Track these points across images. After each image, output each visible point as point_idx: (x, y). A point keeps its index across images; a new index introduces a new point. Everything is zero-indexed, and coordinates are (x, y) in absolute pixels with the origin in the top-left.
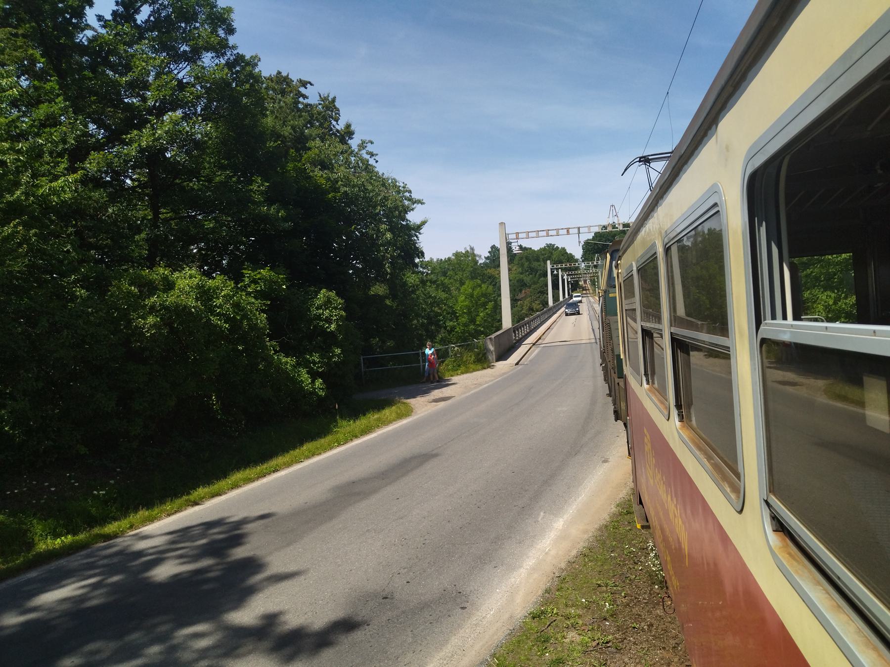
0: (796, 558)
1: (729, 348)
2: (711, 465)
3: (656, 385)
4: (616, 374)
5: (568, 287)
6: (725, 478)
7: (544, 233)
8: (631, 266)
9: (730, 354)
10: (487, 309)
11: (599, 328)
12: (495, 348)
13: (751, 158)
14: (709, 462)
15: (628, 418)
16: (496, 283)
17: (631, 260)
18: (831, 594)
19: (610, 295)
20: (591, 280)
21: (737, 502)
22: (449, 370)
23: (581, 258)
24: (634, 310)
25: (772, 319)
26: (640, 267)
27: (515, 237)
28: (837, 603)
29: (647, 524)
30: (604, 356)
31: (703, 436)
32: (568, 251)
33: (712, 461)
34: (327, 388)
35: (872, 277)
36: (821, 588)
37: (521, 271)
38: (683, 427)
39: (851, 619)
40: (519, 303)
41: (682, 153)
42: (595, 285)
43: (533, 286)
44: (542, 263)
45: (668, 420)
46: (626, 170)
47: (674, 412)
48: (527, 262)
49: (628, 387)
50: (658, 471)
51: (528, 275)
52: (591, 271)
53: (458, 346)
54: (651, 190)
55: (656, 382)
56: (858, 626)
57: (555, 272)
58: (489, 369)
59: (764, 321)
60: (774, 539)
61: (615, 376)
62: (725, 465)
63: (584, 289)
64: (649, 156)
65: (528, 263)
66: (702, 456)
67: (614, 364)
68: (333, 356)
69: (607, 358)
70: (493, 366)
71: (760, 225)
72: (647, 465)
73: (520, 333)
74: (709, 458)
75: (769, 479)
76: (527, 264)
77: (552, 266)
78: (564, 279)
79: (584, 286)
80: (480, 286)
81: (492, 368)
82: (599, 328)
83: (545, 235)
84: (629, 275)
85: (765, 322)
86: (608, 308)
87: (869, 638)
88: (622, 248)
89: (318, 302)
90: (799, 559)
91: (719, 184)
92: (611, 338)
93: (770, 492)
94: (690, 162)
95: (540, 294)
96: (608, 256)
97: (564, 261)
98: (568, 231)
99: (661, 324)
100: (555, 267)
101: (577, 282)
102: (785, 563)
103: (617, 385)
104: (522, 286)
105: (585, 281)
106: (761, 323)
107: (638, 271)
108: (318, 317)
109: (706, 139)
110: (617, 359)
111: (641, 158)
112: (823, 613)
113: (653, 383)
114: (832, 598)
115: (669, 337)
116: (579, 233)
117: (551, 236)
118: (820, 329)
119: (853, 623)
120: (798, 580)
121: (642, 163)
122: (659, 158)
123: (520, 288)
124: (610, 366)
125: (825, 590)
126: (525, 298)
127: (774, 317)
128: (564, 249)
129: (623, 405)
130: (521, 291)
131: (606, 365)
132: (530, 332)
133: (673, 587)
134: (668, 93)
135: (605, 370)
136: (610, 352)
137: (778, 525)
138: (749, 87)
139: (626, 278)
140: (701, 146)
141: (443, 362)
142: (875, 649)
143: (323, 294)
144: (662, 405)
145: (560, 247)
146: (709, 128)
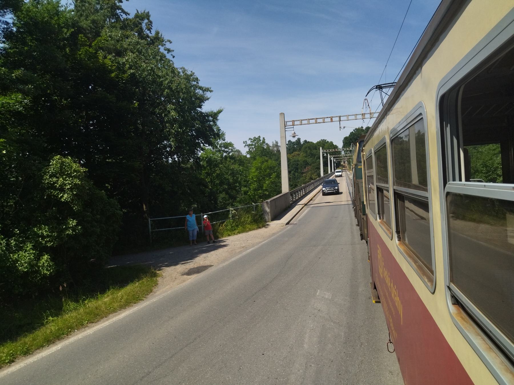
0: (466, 320)
1: (428, 198)
3: (385, 220)
4: (362, 213)
5: (334, 165)
6: (424, 274)
7: (314, 121)
9: (428, 202)
10: (271, 178)
11: (352, 193)
12: (271, 210)
14: (415, 265)
15: (368, 239)
16: (291, 162)
17: (370, 148)
18: (486, 341)
19: (358, 167)
20: (348, 161)
22: (227, 230)
23: (342, 148)
27: (292, 124)
28: (489, 346)
29: (379, 300)
31: (413, 249)
32: (334, 144)
33: (417, 264)
34: (56, 264)
35: (511, 155)
36: (481, 338)
38: (400, 244)
40: (304, 175)
42: (350, 164)
43: (313, 165)
45: (392, 240)
46: (368, 93)
47: (395, 236)
48: (309, 150)
49: (368, 221)
50: (385, 269)
52: (348, 155)
53: (234, 210)
54: (383, 106)
55: (385, 218)
56: (502, 359)
57: (325, 155)
58: (264, 228)
59: (448, 182)
60: (453, 309)
61: (361, 214)
62: (425, 266)
63: (344, 167)
64: (382, 85)
65: (310, 150)
66: (411, 261)
67: (360, 207)
68: (67, 229)
69: (356, 204)
70: (268, 225)
71: (447, 126)
73: (297, 196)
74: (415, 262)
76: (309, 151)
78: (331, 160)
79: (344, 165)
80: (267, 161)
81: (266, 228)
82: (352, 187)
83: (315, 122)
84: (370, 155)
85: (449, 182)
86: (357, 175)
88: (366, 140)
89: (51, 170)
90: (467, 321)
91: (423, 102)
92: (359, 192)
93: (451, 281)
94: (405, 89)
96: (358, 144)
98: (332, 119)
99: (388, 184)
100: (325, 151)
101: (340, 162)
104: (306, 164)
105: (344, 162)
106: (447, 183)
107: (375, 153)
108: (52, 186)
109: (415, 76)
110: (362, 204)
111: (377, 86)
112: (481, 352)
113: (383, 218)
116: (340, 121)
117: (319, 123)
118: (481, 186)
120: (467, 333)
124: (358, 209)
125: (482, 338)
127: (454, 180)
128: (332, 143)
130: (305, 167)
132: (305, 195)
134: (386, 66)
135: (356, 211)
136: (358, 200)
137: (455, 301)
138: (441, 45)
139: (368, 157)
140: (412, 80)
141: (223, 222)
143: (56, 161)
145: (330, 141)
146: (417, 69)
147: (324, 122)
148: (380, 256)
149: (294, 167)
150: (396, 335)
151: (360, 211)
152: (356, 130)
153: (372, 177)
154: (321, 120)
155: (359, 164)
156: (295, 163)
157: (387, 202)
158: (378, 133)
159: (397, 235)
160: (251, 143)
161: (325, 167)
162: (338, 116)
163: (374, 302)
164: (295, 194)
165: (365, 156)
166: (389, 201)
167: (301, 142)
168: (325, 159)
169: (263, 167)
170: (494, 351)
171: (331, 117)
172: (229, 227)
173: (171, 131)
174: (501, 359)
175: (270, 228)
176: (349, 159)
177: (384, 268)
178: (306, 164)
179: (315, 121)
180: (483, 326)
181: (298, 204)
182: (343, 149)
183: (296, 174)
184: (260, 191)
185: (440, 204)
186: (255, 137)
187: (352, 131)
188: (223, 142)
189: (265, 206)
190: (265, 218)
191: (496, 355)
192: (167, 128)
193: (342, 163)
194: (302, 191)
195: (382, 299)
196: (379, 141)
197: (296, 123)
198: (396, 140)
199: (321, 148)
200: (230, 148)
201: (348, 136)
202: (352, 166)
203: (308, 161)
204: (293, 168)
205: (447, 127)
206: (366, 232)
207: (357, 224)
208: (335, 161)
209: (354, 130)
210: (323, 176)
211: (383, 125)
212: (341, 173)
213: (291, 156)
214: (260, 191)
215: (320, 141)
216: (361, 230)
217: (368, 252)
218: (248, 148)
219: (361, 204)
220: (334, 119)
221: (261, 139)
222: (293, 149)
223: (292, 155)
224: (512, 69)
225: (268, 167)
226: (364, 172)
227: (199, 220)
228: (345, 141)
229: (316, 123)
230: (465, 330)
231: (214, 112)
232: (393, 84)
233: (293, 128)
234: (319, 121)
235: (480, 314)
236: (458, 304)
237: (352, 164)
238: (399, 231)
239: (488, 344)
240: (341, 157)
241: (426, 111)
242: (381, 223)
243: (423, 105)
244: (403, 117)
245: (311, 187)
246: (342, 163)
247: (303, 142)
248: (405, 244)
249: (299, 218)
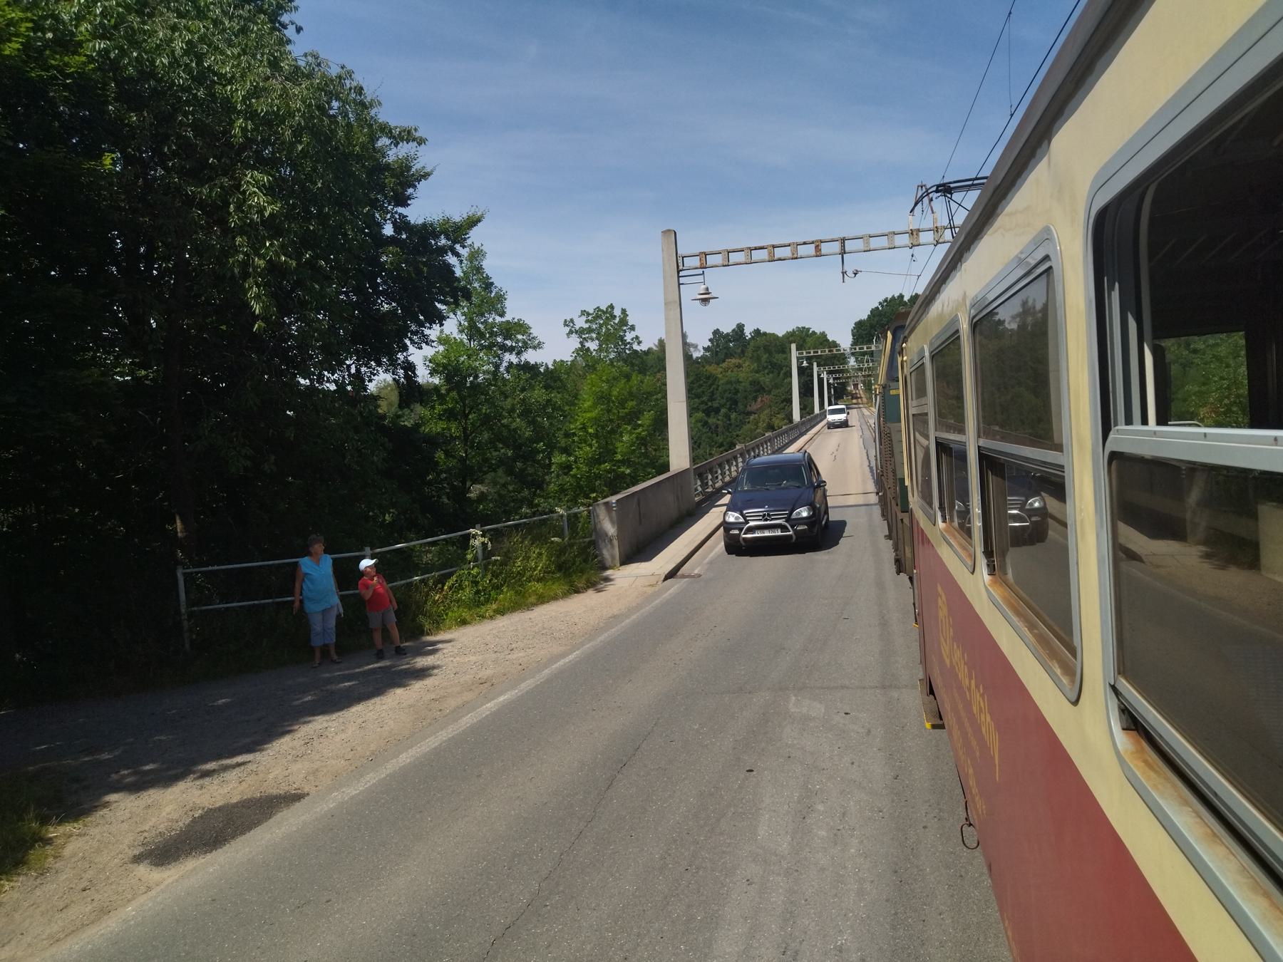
0: (1155, 766)
2: (1034, 636)
4: (899, 507)
5: (829, 392)
6: (1054, 654)
7: (763, 254)
8: (922, 350)
9: (1064, 477)
11: (876, 456)
12: (620, 530)
14: (1031, 633)
15: (915, 571)
16: (718, 386)
17: (920, 345)
18: (1203, 817)
20: (864, 383)
21: (1071, 689)
24: (926, 414)
25: (1126, 424)
26: (935, 352)
27: (698, 264)
28: (1212, 831)
29: (941, 722)
32: (830, 338)
33: (1036, 631)
36: (1190, 809)
37: (756, 368)
38: (994, 582)
39: (1232, 853)
40: (752, 417)
41: (999, 182)
43: (774, 392)
45: (973, 573)
47: (982, 562)
48: (765, 354)
51: (768, 374)
52: (866, 365)
54: (953, 237)
57: (805, 364)
58: (590, 592)
59: (1115, 426)
60: (1124, 740)
61: (897, 509)
63: (854, 396)
64: (950, 183)
65: (767, 355)
67: (896, 492)
71: (1111, 288)
73: (720, 477)
74: (1031, 627)
76: (765, 356)
79: (854, 392)
81: (599, 591)
82: (875, 441)
83: (766, 258)
85: (1117, 428)
86: (889, 413)
87: (1258, 880)
88: (909, 325)
92: (892, 455)
93: (1119, 673)
95: (785, 403)
96: (889, 335)
100: (805, 354)
101: (844, 385)
103: (899, 522)
104: (758, 391)
106: (1110, 430)
107: (933, 357)
109: (1033, 161)
110: (900, 484)
111: (938, 186)
113: (952, 520)
114: (1206, 824)
115: (975, 453)
116: (843, 252)
117: (780, 259)
119: (1235, 859)
121: (939, 194)
122: (968, 185)
124: (890, 495)
126: (760, 410)
127: (1129, 421)
128: (823, 335)
129: (908, 551)
130: (755, 399)
133: (977, 810)
134: (1010, 13)
136: (891, 475)
137: (1130, 721)
142: (1266, 895)
144: (965, 551)
145: (818, 333)
147: (795, 256)
148: (943, 612)
149: (727, 398)
150: (984, 807)
151: (893, 501)
152: (885, 304)
154: (786, 252)
156: (729, 386)
158: (940, 309)
159: (986, 561)
160: (586, 326)
161: (807, 396)
162: (835, 237)
163: (928, 725)
167: (746, 334)
168: (805, 373)
169: (615, 393)
170: (1224, 841)
171: (817, 241)
172: (467, 593)
173: (253, 261)
175: (611, 589)
176: (869, 376)
177: (955, 643)
178: (759, 389)
179: (770, 253)
180: (1168, 750)
181: (717, 504)
183: (733, 416)
184: (606, 464)
185: (1094, 477)
186: (598, 307)
187: (877, 305)
188: (498, 319)
189: (601, 517)
190: (602, 555)
191: (1228, 851)
192: (237, 252)
193: (850, 388)
194: (734, 463)
195: (949, 719)
196: (944, 325)
197: (711, 260)
198: (984, 323)
199: (793, 346)
200: (520, 337)
201: (865, 317)
202: (876, 389)
203: (762, 383)
204: (725, 401)
207: (887, 534)
208: (831, 381)
209: (880, 303)
210: (799, 420)
211: (965, 270)
212: (845, 415)
213: (721, 370)
214: (607, 466)
215: (793, 330)
216: (896, 549)
217: (914, 604)
218: (579, 340)
220: (825, 248)
221: (617, 312)
222: (725, 351)
223: (721, 367)
224: (1276, 143)
225: (631, 394)
226: (908, 407)
227: (346, 575)
228: (858, 331)
230: (1152, 792)
231: (455, 223)
232: (976, 182)
233: (702, 276)
234: (779, 253)
235: (1190, 750)
236: (1137, 729)
237: (874, 384)
239: (1209, 827)
240: (847, 371)
241: (1060, 248)
242: (946, 531)
244: (1030, 237)
245: (763, 450)
246: (850, 388)
247: (750, 334)
248: (1006, 583)
249: (712, 555)
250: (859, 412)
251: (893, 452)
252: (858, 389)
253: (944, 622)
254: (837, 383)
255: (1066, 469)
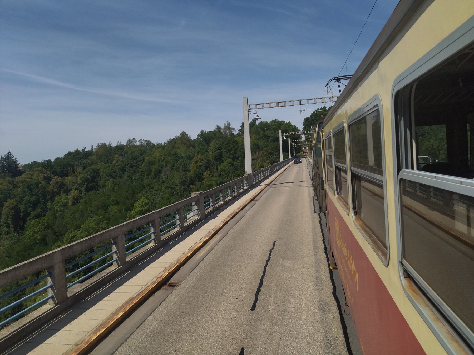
9: (383, 185)
11: (312, 170)
13: (397, 82)
15: (327, 212)
18: (434, 312)
23: (303, 131)
25: (406, 169)
26: (334, 133)
28: (437, 316)
29: (336, 267)
30: (314, 179)
32: (293, 124)
33: (372, 238)
36: (429, 308)
38: (356, 219)
41: (359, 76)
44: (273, 131)
46: (261, 284)
48: (262, 131)
49: (327, 195)
54: (340, 94)
55: (342, 194)
57: (285, 138)
60: (404, 281)
63: (304, 152)
64: (340, 77)
67: (319, 183)
72: (337, 237)
74: (370, 237)
75: (403, 251)
77: (283, 134)
79: (304, 150)
86: (317, 154)
92: (318, 169)
93: (403, 258)
95: (270, 155)
96: (317, 125)
97: (290, 131)
100: (285, 134)
102: (410, 294)
103: (321, 193)
104: (257, 149)
107: (334, 135)
111: (335, 78)
113: (341, 194)
114: (435, 314)
116: (300, 104)
119: (445, 328)
122: (345, 78)
123: (255, 150)
124: (317, 184)
125: (431, 309)
129: (324, 203)
131: (315, 183)
137: (407, 274)
142: (457, 342)
151: (319, 186)
153: (330, 156)
155: (318, 143)
157: (344, 183)
162: (298, 100)
164: (258, 175)
165: (325, 137)
166: (347, 182)
170: (441, 321)
174: (448, 328)
182: (303, 132)
204: (241, 153)
205: (402, 120)
206: (324, 205)
216: (320, 203)
217: (326, 224)
219: (320, 179)
229: (278, 106)
236: (409, 278)
238: (356, 208)
239: (435, 315)
241: (446, 327)
243: (380, 98)
248: (361, 220)
250: (307, 160)
251: (318, 167)
252: (306, 149)
253: (338, 231)
254: (296, 146)
255: (384, 182)
